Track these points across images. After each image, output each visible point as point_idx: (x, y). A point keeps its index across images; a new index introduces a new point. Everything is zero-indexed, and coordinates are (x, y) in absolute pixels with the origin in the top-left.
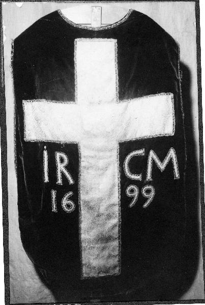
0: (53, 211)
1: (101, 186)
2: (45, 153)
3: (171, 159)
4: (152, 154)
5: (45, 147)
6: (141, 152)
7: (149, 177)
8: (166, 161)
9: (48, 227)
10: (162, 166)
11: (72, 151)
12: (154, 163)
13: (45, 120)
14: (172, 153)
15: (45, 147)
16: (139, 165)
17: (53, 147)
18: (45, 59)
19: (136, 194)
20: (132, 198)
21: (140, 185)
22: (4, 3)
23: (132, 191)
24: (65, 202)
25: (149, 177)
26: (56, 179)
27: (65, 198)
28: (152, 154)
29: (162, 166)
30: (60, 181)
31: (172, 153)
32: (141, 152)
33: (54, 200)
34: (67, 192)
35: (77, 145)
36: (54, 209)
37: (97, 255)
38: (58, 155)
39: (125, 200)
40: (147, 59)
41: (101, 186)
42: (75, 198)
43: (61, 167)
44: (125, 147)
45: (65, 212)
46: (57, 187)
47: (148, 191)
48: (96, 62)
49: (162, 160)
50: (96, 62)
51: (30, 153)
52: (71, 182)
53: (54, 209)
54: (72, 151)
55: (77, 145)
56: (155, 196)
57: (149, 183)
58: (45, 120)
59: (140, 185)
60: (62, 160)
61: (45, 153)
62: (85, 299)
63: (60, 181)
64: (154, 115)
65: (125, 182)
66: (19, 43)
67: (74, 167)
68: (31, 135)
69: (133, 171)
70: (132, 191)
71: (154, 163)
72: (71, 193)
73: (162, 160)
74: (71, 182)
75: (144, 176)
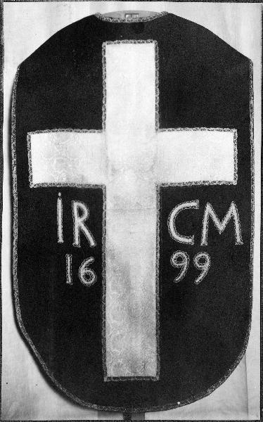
0: (67, 282)
1: (131, 248)
2: (60, 202)
3: (232, 218)
4: (209, 209)
5: (60, 194)
6: (194, 204)
7: (204, 241)
8: (225, 222)
9: (61, 313)
10: (221, 227)
11: (94, 197)
12: (210, 219)
13: (54, 157)
14: (233, 210)
15: (60, 194)
16: (189, 223)
17: (70, 193)
18: (64, 82)
19: (185, 264)
20: (179, 270)
21: (191, 251)
22: (5, 4)
23: (180, 259)
24: (83, 271)
25: (204, 241)
26: (72, 240)
27: (84, 266)
28: (209, 209)
29: (221, 227)
30: (77, 242)
31: (233, 210)
32: (194, 204)
33: (69, 268)
34: (88, 257)
35: (101, 128)
36: (69, 280)
37: (130, 344)
38: (76, 205)
39: (165, 271)
40: (199, 84)
41: (131, 248)
42: (98, 267)
43: (79, 222)
44: (169, 196)
45: (82, 284)
46: (73, 251)
47: (202, 261)
48: (131, 71)
49: (221, 218)
50: (131, 71)
51: (37, 207)
52: (93, 243)
53: (69, 280)
54: (94, 197)
55: (101, 128)
56: (210, 269)
57: (204, 249)
58: (54, 157)
59: (191, 251)
60: (81, 213)
61: (60, 202)
62: (107, 167)
63: (77, 242)
64: (207, 155)
65: (166, 246)
66: (25, 69)
67: (96, 223)
68: (41, 175)
69: (180, 230)
70: (180, 259)
71: (210, 219)
72: (92, 259)
73: (221, 218)
74: (93, 243)
75: (198, 239)
